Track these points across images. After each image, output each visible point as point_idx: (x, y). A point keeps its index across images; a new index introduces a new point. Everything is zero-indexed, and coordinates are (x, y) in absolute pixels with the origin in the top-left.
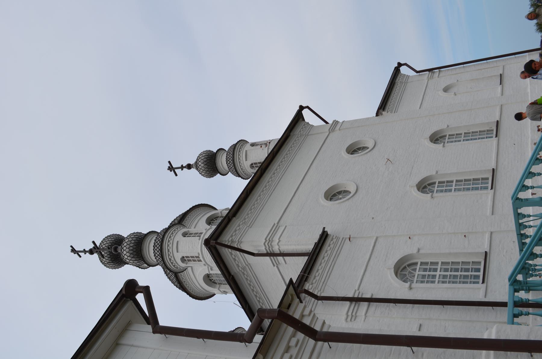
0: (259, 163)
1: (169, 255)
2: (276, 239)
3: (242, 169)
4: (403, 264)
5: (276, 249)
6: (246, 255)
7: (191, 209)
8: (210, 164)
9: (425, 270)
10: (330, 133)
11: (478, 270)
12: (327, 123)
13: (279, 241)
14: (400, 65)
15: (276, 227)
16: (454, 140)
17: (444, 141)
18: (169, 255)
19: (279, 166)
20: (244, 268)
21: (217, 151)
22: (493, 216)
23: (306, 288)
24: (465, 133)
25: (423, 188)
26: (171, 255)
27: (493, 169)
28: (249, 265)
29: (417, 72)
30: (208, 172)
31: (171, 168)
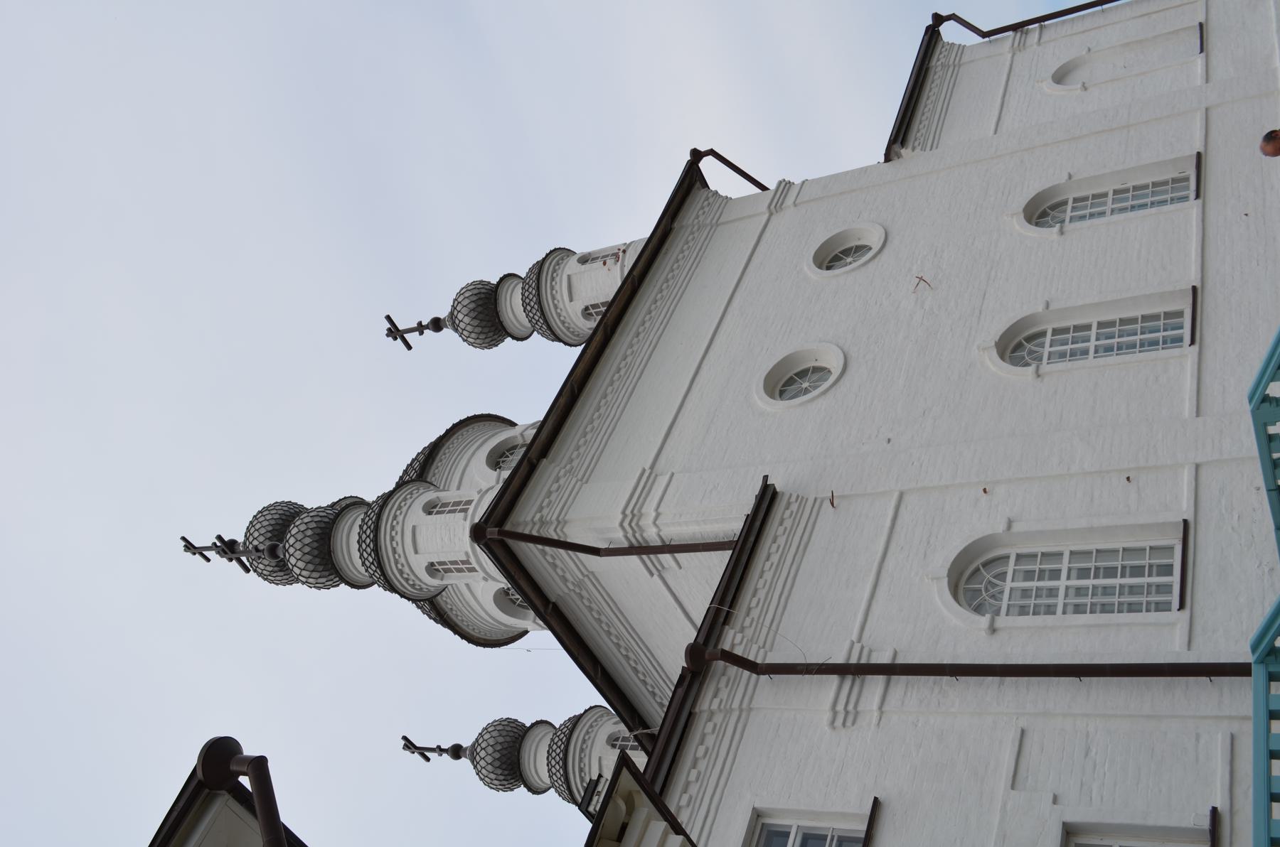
0: (603, 304)
1: (396, 562)
2: (649, 510)
3: (563, 323)
4: (971, 562)
5: (651, 536)
6: (582, 556)
7: (448, 432)
8: (484, 316)
9: (1029, 575)
10: (771, 214)
11: (1167, 570)
13: (658, 515)
14: (938, 19)
15: (648, 477)
16: (1087, 212)
17: (1062, 216)
18: (396, 562)
19: (650, 312)
20: (579, 584)
22: (1200, 419)
23: (727, 647)
24: (1116, 192)
25: (1014, 350)
26: (402, 560)
27: (1194, 288)
28: (591, 575)
29: (984, 35)
30: (482, 336)
31: (394, 332)
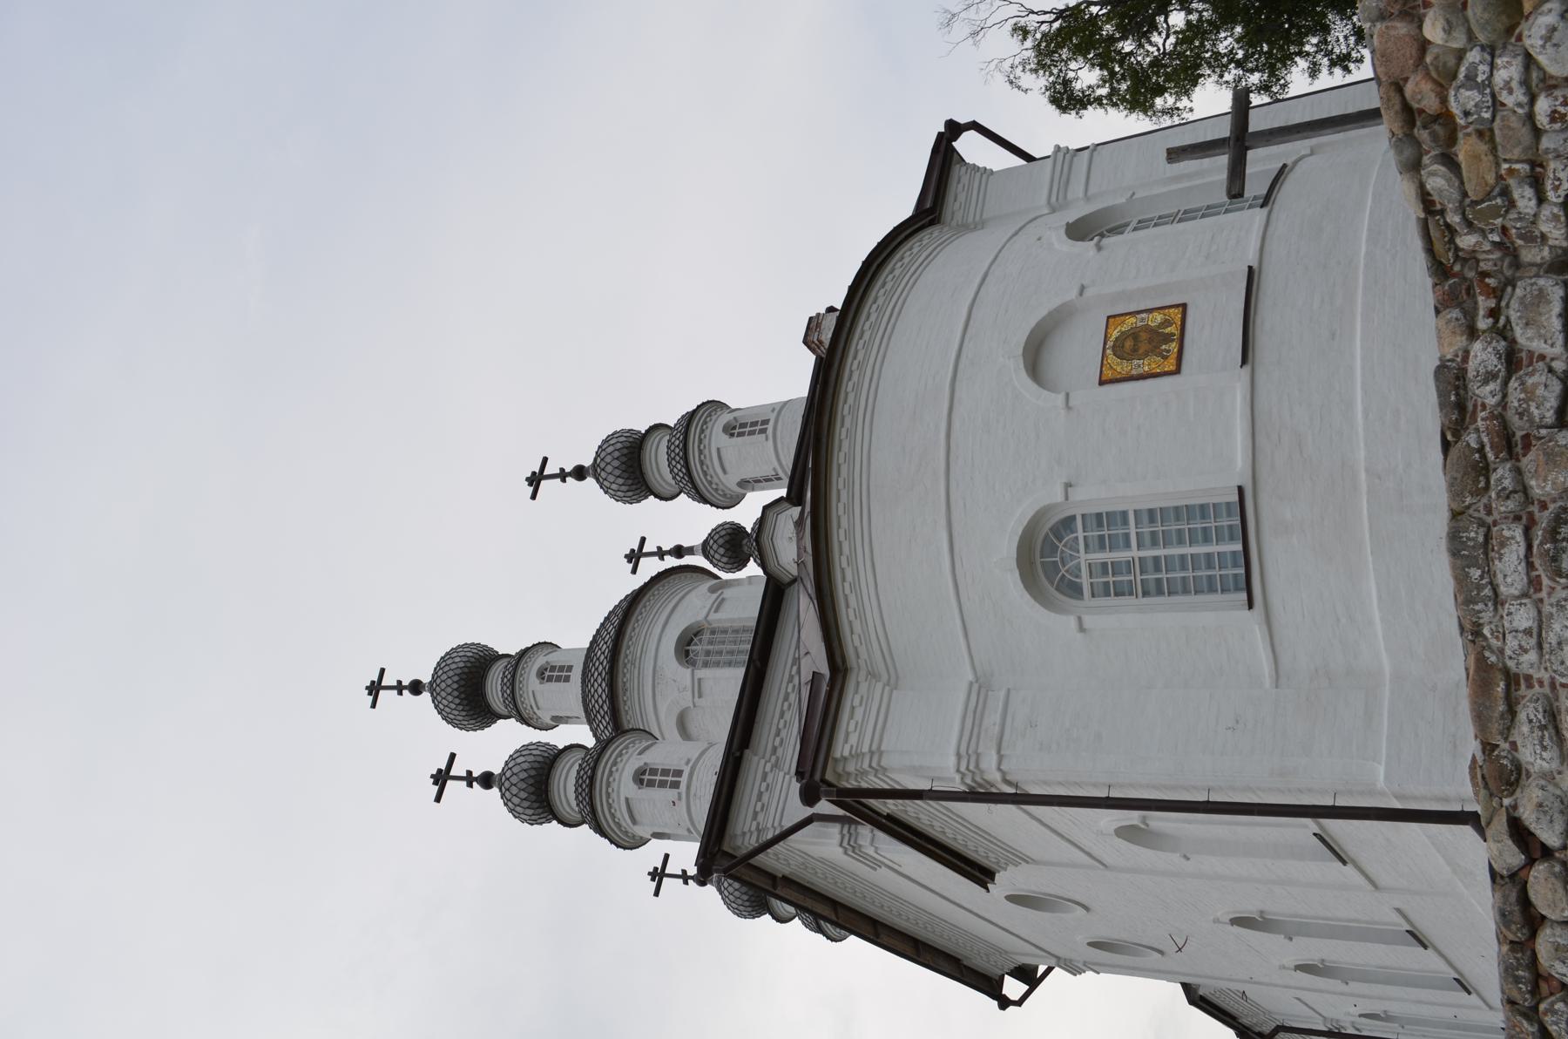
5: (993, 777)
12: (1028, 157)
13: (1001, 758)
21: (648, 431)
